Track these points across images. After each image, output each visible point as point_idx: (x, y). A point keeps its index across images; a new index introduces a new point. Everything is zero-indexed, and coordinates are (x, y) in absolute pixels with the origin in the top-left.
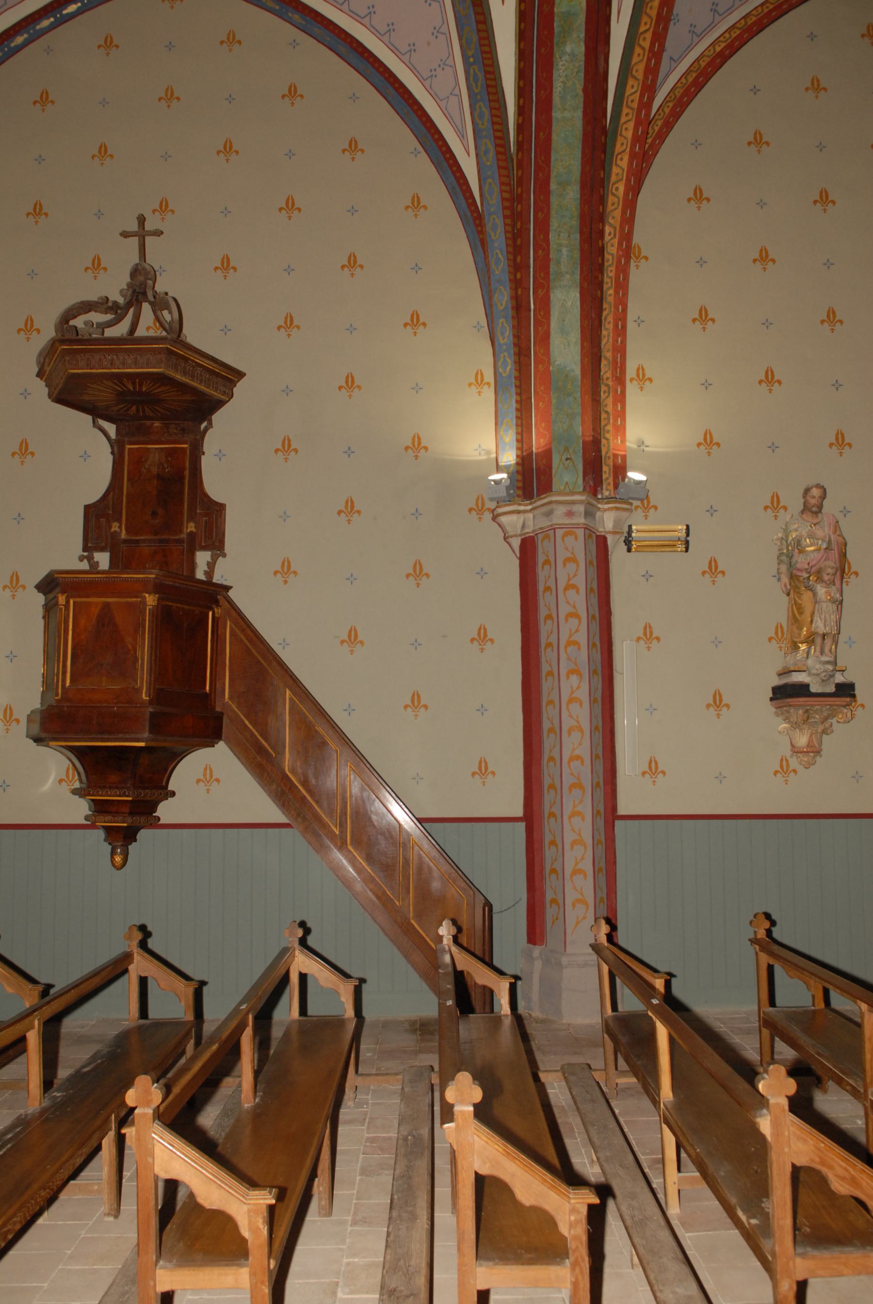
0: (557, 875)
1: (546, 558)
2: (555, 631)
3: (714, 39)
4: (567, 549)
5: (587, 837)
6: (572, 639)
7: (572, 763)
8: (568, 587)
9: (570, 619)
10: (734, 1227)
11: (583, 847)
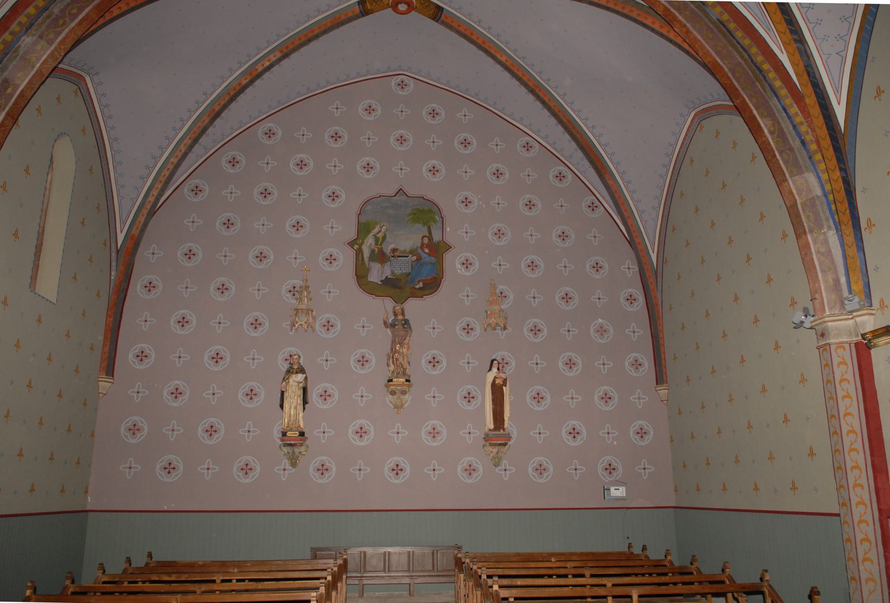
0: (842, 471)
1: (826, 363)
2: (840, 440)
3: (811, 48)
4: (843, 390)
5: (853, 393)
6: (843, 377)
7: (851, 453)
8: (851, 450)
9: (841, 366)
10: (734, 4)
11: (855, 435)
